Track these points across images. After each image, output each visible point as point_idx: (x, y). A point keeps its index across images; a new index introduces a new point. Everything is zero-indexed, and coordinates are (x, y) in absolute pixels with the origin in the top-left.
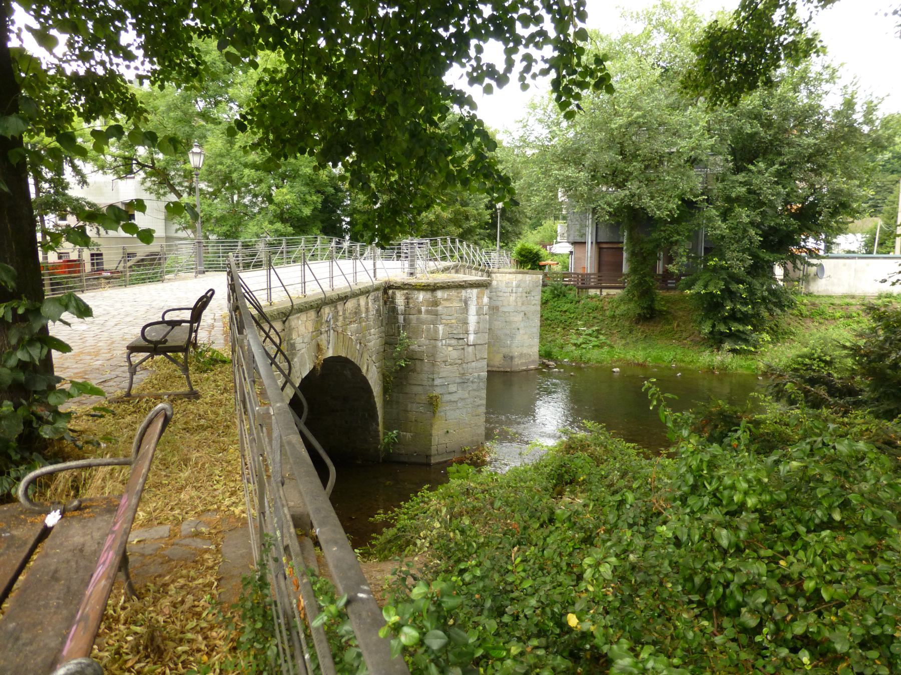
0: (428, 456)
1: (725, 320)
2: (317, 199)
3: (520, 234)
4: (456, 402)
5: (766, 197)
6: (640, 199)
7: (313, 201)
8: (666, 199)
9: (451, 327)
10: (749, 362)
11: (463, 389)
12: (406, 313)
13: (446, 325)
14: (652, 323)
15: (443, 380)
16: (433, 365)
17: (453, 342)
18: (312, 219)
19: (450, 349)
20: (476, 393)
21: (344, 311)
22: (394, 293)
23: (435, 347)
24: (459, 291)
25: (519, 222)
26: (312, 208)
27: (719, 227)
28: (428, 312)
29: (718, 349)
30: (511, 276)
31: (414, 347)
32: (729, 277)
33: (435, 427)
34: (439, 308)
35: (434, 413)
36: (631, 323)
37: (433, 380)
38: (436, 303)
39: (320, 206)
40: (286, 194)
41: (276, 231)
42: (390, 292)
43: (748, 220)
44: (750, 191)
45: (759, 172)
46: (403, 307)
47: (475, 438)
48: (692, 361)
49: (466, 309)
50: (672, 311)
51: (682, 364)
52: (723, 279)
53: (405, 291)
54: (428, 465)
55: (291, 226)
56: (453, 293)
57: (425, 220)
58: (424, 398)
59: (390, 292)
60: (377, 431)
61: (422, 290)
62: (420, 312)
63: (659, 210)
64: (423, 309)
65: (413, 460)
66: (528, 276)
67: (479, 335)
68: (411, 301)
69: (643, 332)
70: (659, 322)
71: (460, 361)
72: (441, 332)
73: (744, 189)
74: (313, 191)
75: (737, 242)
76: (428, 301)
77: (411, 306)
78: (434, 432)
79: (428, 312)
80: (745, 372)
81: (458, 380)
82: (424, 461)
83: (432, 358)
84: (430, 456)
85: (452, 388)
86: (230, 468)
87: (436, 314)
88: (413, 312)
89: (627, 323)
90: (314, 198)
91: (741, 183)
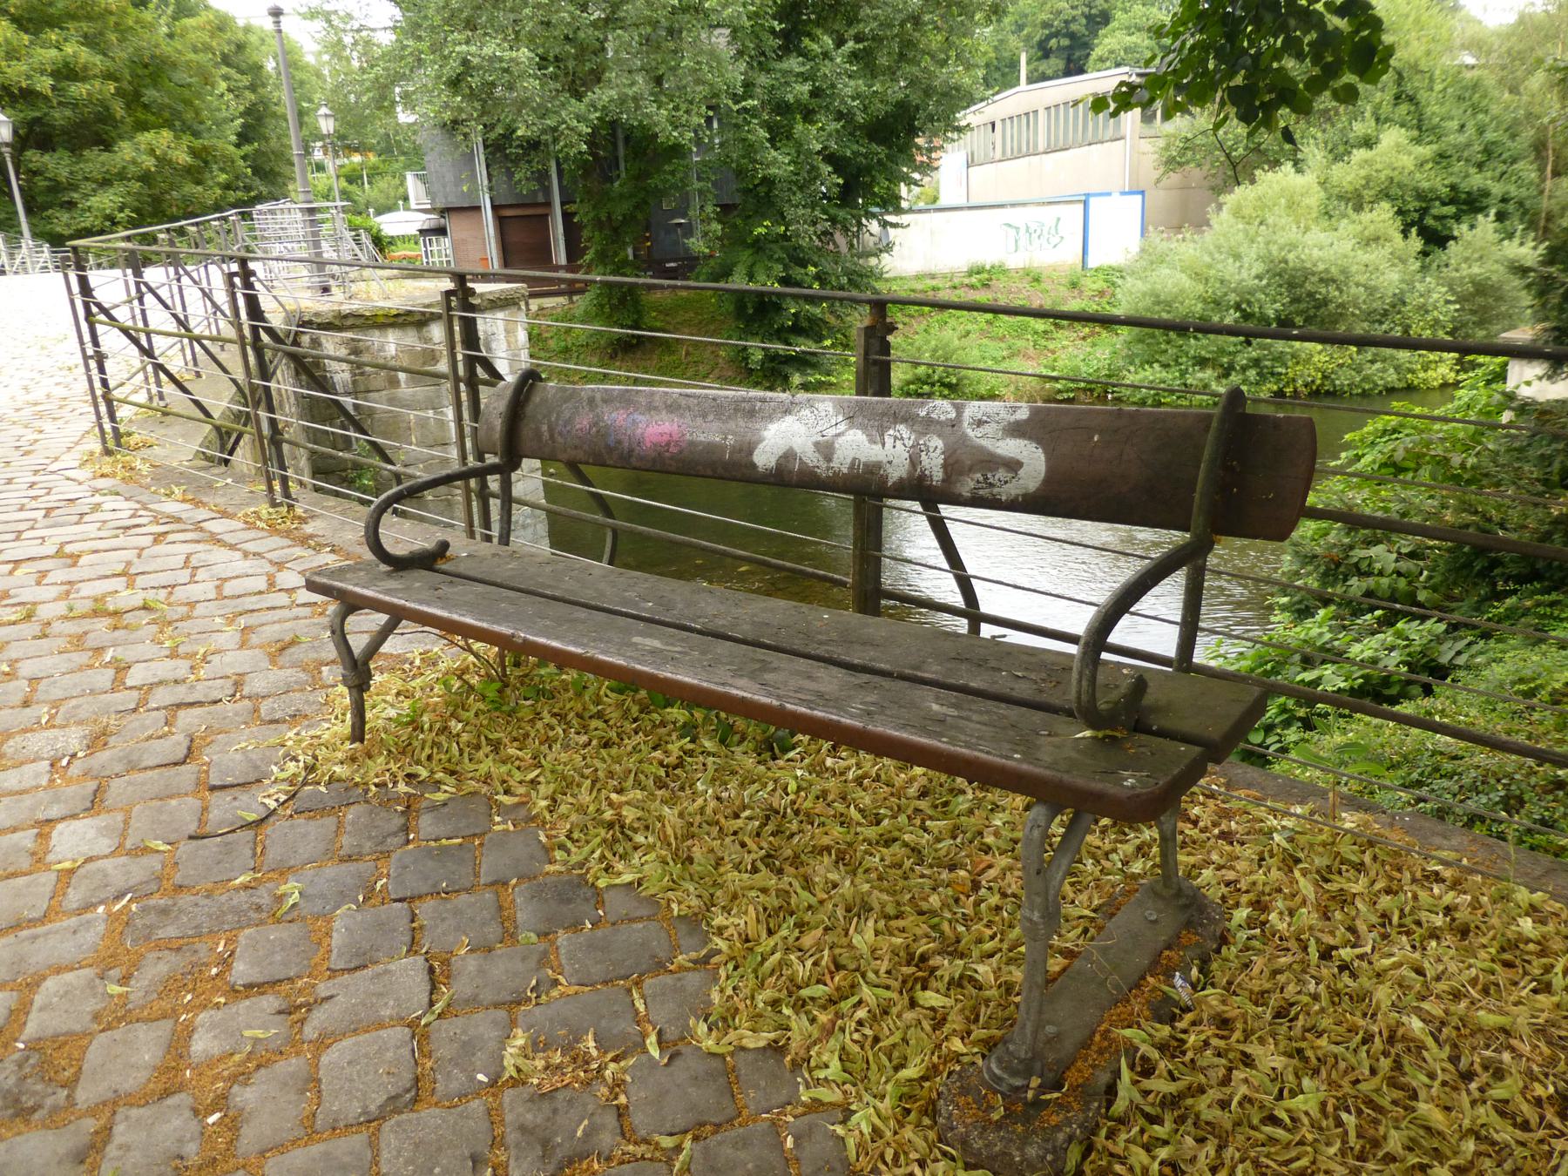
1: (782, 335)
5: (843, 102)
6: (638, 107)
8: (684, 107)
14: (639, 354)
25: (279, 174)
27: (775, 161)
43: (819, 147)
44: (815, 93)
45: (826, 55)
52: (779, 260)
53: (349, 335)
57: (132, 168)
61: (393, 325)
73: (807, 87)
75: (801, 188)
86: (961, 929)
91: (799, 75)
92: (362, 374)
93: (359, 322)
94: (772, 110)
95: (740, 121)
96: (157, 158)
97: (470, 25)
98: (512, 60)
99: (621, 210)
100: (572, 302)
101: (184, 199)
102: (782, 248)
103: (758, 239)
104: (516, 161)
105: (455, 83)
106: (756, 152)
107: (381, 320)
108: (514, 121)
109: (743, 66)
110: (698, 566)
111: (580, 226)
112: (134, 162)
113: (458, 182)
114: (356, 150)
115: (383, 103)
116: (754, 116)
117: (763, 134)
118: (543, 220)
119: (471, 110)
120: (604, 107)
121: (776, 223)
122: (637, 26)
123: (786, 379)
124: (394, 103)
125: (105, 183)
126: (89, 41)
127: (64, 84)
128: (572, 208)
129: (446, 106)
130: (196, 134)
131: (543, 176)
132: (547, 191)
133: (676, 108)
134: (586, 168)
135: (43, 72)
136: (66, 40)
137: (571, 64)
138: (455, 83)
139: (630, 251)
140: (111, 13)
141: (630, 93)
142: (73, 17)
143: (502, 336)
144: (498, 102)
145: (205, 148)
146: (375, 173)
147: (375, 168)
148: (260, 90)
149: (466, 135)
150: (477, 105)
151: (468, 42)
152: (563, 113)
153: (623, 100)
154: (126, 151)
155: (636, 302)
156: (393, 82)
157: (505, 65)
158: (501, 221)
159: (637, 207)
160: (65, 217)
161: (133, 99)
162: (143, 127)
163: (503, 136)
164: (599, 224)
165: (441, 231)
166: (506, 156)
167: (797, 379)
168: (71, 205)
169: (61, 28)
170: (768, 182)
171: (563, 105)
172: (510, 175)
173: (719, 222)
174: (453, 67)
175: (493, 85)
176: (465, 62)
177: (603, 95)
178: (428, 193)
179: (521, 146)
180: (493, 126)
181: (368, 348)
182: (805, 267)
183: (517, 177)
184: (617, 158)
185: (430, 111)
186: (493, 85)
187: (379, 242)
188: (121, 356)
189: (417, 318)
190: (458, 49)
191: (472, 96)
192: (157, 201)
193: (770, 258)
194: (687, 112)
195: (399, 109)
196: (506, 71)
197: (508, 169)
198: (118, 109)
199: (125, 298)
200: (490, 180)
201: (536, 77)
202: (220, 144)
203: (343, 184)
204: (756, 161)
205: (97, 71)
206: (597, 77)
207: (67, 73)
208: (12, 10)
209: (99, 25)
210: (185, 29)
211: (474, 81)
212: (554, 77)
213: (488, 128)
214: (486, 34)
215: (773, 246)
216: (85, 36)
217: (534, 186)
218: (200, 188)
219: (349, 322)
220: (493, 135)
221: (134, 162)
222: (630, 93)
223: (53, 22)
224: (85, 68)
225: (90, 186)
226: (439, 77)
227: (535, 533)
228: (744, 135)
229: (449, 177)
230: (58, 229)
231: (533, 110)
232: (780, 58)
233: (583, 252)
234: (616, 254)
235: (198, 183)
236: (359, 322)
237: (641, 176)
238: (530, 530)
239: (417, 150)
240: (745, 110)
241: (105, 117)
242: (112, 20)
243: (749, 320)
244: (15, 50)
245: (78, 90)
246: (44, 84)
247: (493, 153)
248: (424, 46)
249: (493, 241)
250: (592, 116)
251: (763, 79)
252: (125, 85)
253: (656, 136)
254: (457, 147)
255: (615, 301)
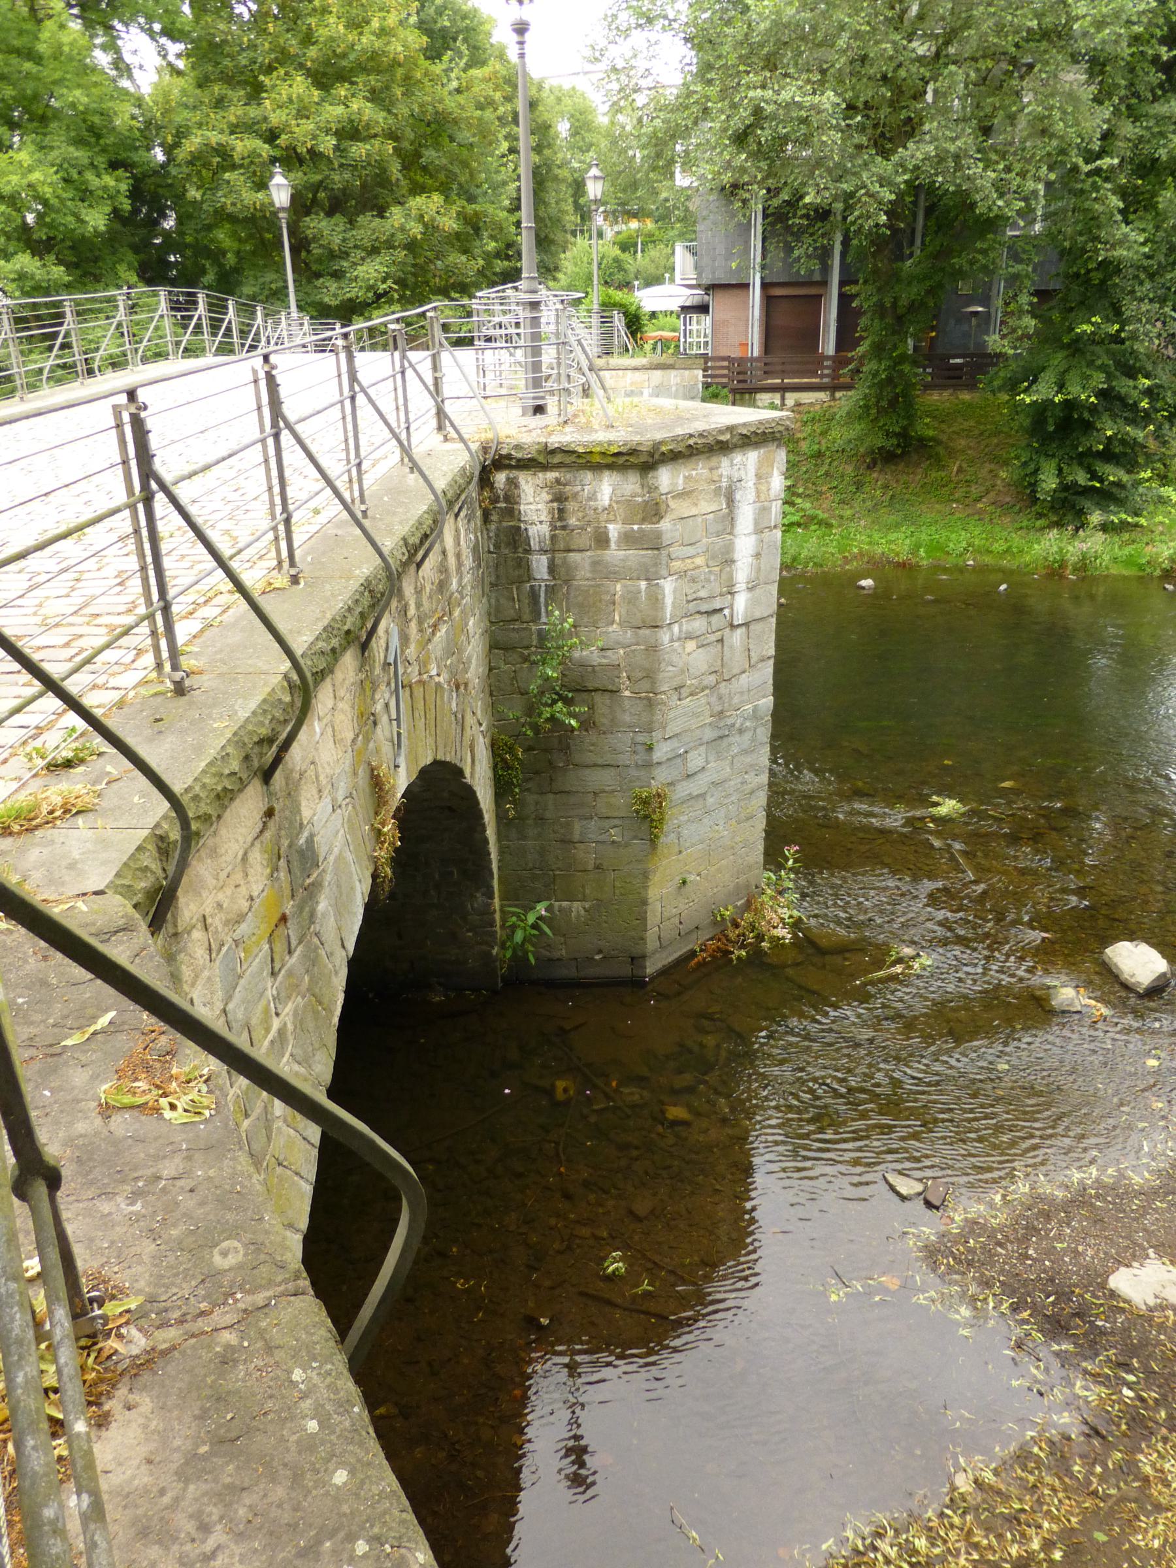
0: (637, 960)
1: (1085, 459)
2: (116, 183)
3: (557, 269)
4: (702, 796)
6: (958, 167)
7: (105, 188)
8: (1017, 167)
9: (693, 580)
10: (1127, 550)
11: (719, 758)
12: (556, 547)
13: (682, 574)
14: (901, 466)
15: (674, 743)
16: (650, 704)
17: (698, 624)
18: (111, 239)
19: (691, 645)
20: (748, 760)
21: (419, 592)
22: (512, 483)
23: (653, 649)
24: (714, 461)
25: (552, 242)
26: (108, 209)
28: (629, 539)
29: (1082, 526)
30: (639, 376)
31: (591, 655)
32: (1118, 364)
33: (655, 878)
34: (665, 525)
35: (653, 841)
36: (857, 468)
37: (650, 749)
38: (654, 510)
39: (126, 205)
40: (30, 170)
41: (21, 277)
42: (500, 478)
46: (545, 529)
47: (742, 879)
48: (1008, 551)
49: (729, 518)
50: (944, 438)
51: (987, 559)
52: (1102, 368)
53: (551, 475)
54: (637, 983)
55: (60, 262)
56: (699, 470)
58: (621, 803)
59: (500, 478)
60: (487, 912)
61: (610, 467)
62: (602, 540)
63: (1001, 195)
64: (614, 530)
65: (592, 972)
66: (673, 373)
67: (758, 591)
68: (571, 506)
69: (886, 487)
70: (918, 465)
71: (712, 679)
72: (669, 601)
74: (101, 161)
75: (1152, 277)
76: (629, 503)
77: (572, 521)
78: (653, 893)
79: (629, 539)
80: (1126, 573)
81: (709, 734)
82: (626, 971)
83: (645, 685)
84: (644, 957)
85: (696, 760)
87: (655, 544)
88: (582, 540)
89: (849, 469)
90: (109, 180)
92: (564, 528)
93: (568, 460)
94: (1133, 172)
95: (1087, 186)
96: (425, 225)
97: (770, 64)
98: (813, 107)
99: (908, 294)
100: (833, 399)
101: (449, 271)
102: (1108, 352)
103: (1079, 338)
104: (799, 234)
105: (741, 139)
106: (1099, 227)
107: (597, 459)
108: (804, 184)
109: (1106, 112)
110: (947, 767)
111: (859, 313)
112: (402, 229)
113: (729, 256)
114: (634, 215)
115: (662, 163)
116: (1107, 180)
117: (1116, 202)
118: (815, 301)
119: (756, 170)
120: (916, 167)
121: (1107, 319)
122: (974, 59)
123: (1081, 513)
124: (672, 162)
125: (374, 251)
126: (375, 96)
127: (345, 144)
128: (851, 289)
129: (728, 165)
130: (471, 199)
131: (824, 254)
132: (826, 269)
133: (1008, 169)
134: (877, 241)
135: (327, 132)
136: (353, 95)
137: (884, 112)
138: (741, 139)
139: (910, 342)
140: (400, 65)
141: (953, 148)
142: (366, 70)
143: (750, 483)
144: (787, 162)
145: (476, 214)
146: (651, 240)
147: (650, 235)
148: (546, 152)
149: (745, 202)
150: (764, 165)
151: (763, 87)
152: (865, 175)
153: (940, 159)
154: (396, 216)
155: (909, 404)
156: (673, 137)
157: (803, 113)
158: (769, 301)
159: (930, 292)
160: (333, 286)
161: (410, 160)
162: (418, 189)
163: (787, 203)
164: (880, 310)
165: (703, 309)
166: (788, 228)
167: (1096, 518)
168: (338, 275)
169: (352, 83)
170: (1110, 268)
171: (866, 164)
172: (789, 250)
173: (1034, 316)
174: (744, 115)
175: (785, 140)
176: (757, 112)
177: (916, 152)
178: (696, 267)
179: (807, 216)
180: (778, 191)
181: (575, 495)
182: (1135, 379)
183: (796, 253)
184: (913, 231)
185: (706, 169)
186: (785, 140)
187: (634, 323)
188: (372, 431)
189: (643, 459)
190: (751, 94)
191: (758, 154)
192: (421, 270)
193: (1091, 364)
194: (1023, 174)
195: (678, 170)
196: (805, 121)
197: (787, 244)
198: (395, 169)
199: (337, 398)
200: (764, 256)
201: (837, 128)
202: (491, 209)
203: (617, 252)
204: (1096, 239)
205: (378, 130)
206: (910, 129)
207: (350, 132)
208: (309, 64)
209: (387, 77)
210: (471, 80)
211: (764, 135)
212: (861, 128)
213: (772, 192)
214: (786, 75)
215: (1098, 349)
216: (373, 91)
217: (815, 265)
218: (464, 258)
219: (556, 459)
220: (776, 202)
221: (402, 229)
222: (952, 148)
223: (344, 76)
224: (368, 126)
225: (360, 253)
226: (725, 130)
227: (753, 740)
228: (1087, 204)
229: (721, 249)
230: (326, 299)
231: (829, 171)
232: (1156, 99)
233: (857, 343)
234: (895, 348)
235: (465, 252)
236: (568, 460)
237: (943, 254)
238: (747, 736)
239: (688, 219)
240: (1098, 172)
241: (382, 179)
242: (400, 72)
243: (1046, 439)
244: (305, 108)
245: (359, 150)
246: (327, 144)
247: (772, 224)
248: (713, 91)
249: (757, 324)
250: (899, 179)
251: (1128, 129)
252: (406, 144)
253: (973, 205)
254: (733, 216)
255: (884, 403)
